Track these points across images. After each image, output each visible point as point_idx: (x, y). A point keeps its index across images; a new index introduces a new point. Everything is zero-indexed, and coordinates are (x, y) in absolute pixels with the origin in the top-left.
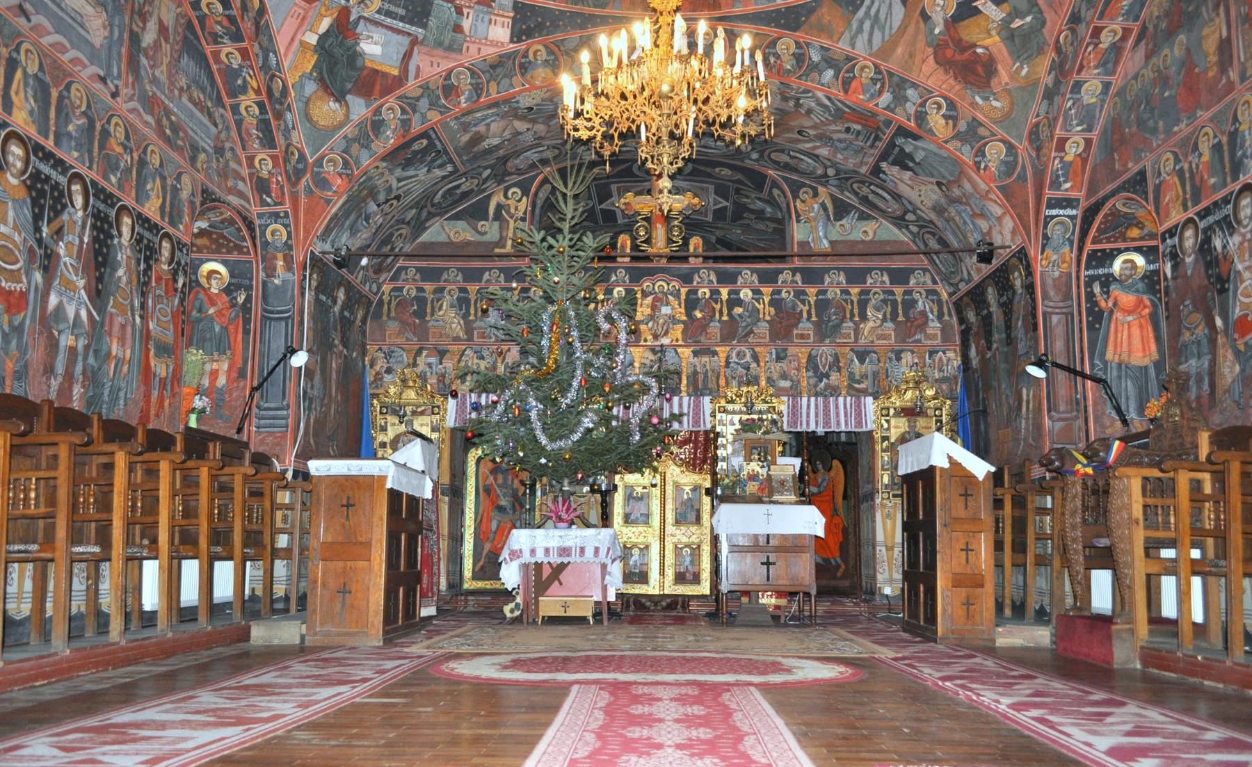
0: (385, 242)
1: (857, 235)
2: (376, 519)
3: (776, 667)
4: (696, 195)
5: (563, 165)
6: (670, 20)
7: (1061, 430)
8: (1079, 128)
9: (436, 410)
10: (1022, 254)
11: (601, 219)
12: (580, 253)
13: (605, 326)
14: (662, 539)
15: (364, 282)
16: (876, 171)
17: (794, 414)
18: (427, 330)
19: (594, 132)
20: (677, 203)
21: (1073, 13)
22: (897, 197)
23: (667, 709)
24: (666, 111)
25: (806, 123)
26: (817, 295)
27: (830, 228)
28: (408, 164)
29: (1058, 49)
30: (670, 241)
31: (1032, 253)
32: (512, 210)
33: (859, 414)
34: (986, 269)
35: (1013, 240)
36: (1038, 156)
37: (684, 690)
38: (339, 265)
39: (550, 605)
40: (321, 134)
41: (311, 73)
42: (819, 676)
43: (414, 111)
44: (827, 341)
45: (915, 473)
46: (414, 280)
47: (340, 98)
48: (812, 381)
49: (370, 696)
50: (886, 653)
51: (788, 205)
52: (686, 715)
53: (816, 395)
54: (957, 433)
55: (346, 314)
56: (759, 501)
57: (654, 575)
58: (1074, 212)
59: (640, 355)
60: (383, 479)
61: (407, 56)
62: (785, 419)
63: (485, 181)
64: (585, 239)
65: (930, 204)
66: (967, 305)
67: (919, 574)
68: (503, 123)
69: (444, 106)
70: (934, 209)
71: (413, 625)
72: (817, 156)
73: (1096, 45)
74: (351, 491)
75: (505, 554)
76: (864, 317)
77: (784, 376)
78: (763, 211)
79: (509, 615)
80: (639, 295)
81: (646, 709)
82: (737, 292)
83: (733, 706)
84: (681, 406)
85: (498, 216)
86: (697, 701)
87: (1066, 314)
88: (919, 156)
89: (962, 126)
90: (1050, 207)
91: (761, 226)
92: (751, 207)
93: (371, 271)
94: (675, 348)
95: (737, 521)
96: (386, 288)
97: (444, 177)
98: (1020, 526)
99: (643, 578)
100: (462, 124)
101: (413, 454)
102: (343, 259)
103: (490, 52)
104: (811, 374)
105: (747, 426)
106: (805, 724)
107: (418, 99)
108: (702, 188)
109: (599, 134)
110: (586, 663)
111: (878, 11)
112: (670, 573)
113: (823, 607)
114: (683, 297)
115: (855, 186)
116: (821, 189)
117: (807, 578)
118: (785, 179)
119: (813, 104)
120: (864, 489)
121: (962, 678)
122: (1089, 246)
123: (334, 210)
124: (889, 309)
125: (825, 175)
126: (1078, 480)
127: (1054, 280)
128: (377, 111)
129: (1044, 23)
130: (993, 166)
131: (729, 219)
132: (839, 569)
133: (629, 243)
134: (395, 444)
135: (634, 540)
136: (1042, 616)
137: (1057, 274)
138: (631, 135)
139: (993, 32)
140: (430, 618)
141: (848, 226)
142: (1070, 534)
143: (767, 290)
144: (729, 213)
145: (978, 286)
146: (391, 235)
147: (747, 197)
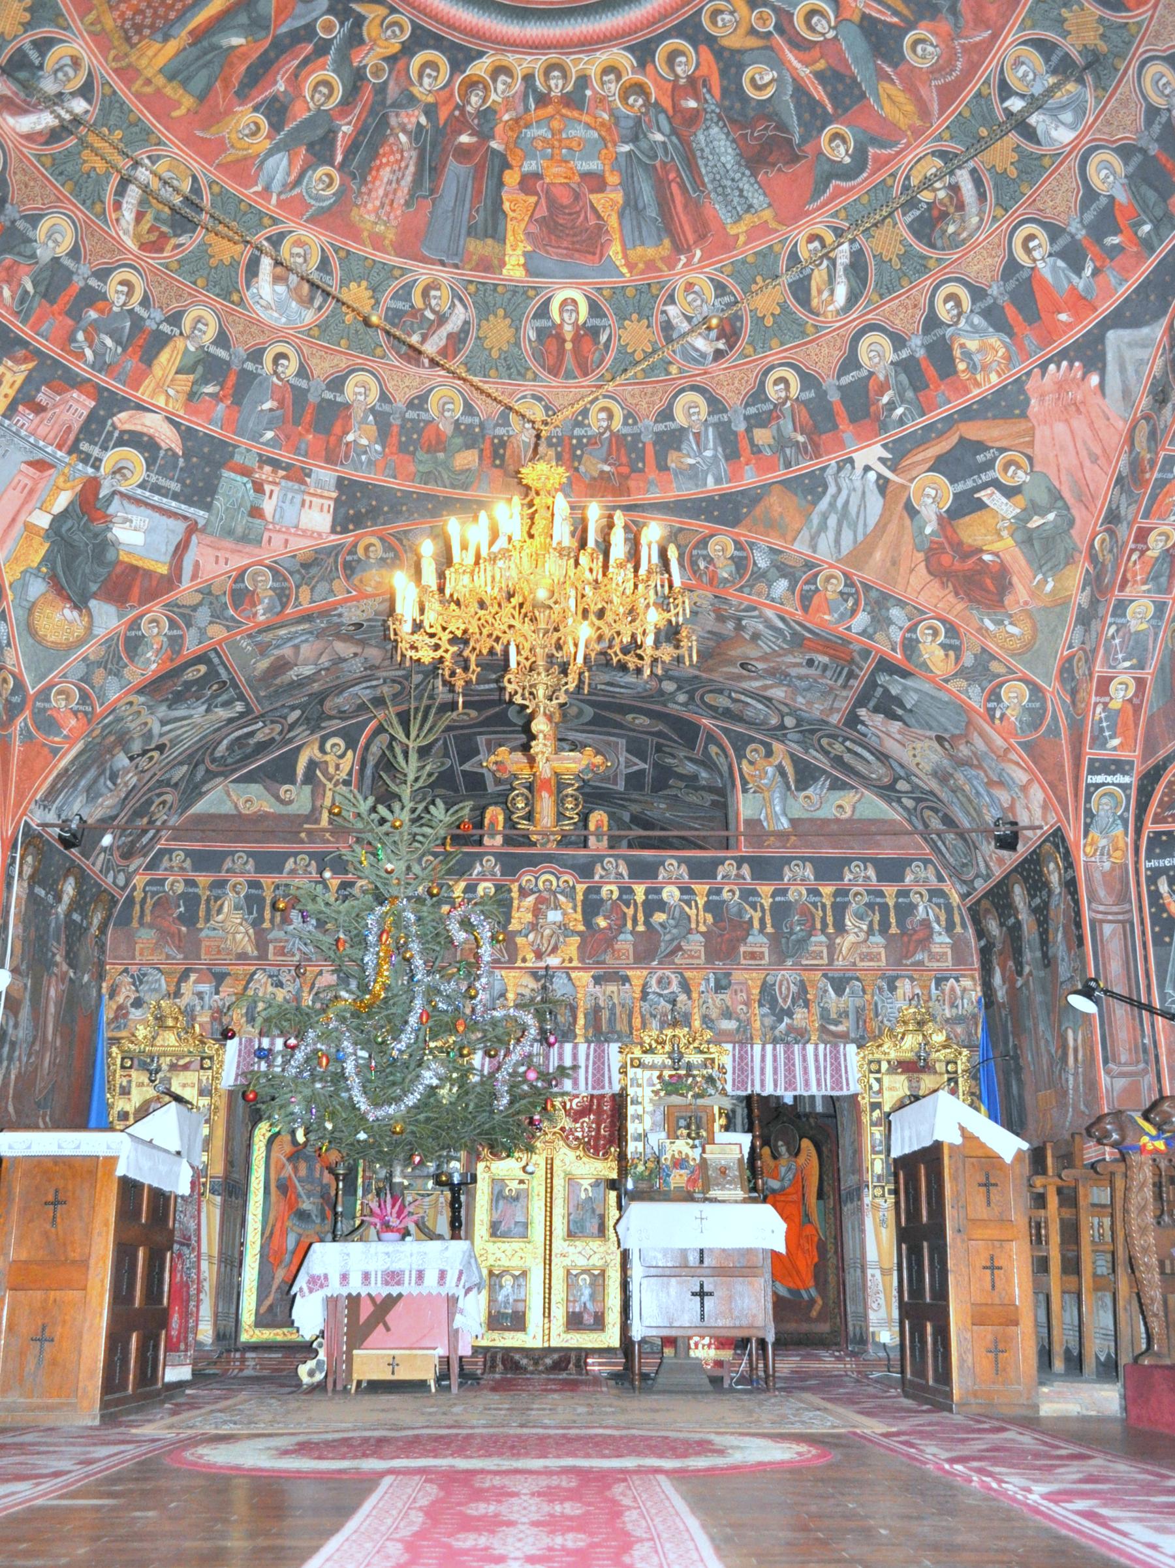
0: (138, 813)
1: (828, 811)
2: (98, 1224)
3: (703, 1447)
4: (598, 752)
5: (404, 707)
6: (549, 501)
7: (1125, 1090)
8: (1127, 664)
9: (207, 1063)
10: (1057, 838)
11: (461, 784)
12: (427, 830)
13: (460, 936)
14: (548, 1261)
15: (106, 869)
16: (853, 720)
17: (742, 1070)
18: (197, 943)
19: (440, 653)
20: (573, 763)
21: (1110, 510)
22: (883, 757)
23: (525, 1507)
24: (542, 625)
25: (753, 652)
26: (773, 896)
27: (791, 801)
28: (177, 699)
29: (1093, 557)
30: (560, 816)
31: (1071, 835)
32: (331, 770)
33: (837, 1069)
34: (1011, 859)
35: (1044, 817)
36: (1073, 703)
37: (555, 1481)
38: (67, 843)
39: (370, 1363)
40: (49, 655)
41: (38, 569)
42: (766, 1458)
43: (189, 625)
44: (789, 963)
45: (914, 1154)
46: (182, 869)
47: (80, 604)
48: (769, 1021)
49: (61, 1497)
50: (873, 1427)
51: (730, 767)
52: (552, 1516)
53: (775, 1041)
54: (980, 1098)
55: (76, 917)
56: (689, 1198)
57: (534, 1317)
58: (1126, 780)
59: (517, 983)
60: (112, 1161)
61: (181, 548)
62: (729, 1077)
63: (292, 727)
64: (432, 808)
65: (928, 768)
66: (987, 911)
67: (924, 1310)
68: (319, 645)
69: (233, 619)
70: (935, 774)
71: (147, 1396)
72: (770, 699)
73: (1143, 553)
74: (61, 1181)
75: (301, 1282)
76: (841, 929)
77: (727, 1014)
78: (695, 777)
79: (306, 1379)
80: (515, 895)
81: (492, 1508)
82: (658, 891)
83: (627, 1501)
84: (575, 1056)
85: (309, 778)
86: (573, 1495)
87: (1122, 922)
88: (910, 700)
89: (968, 660)
90: (1093, 771)
91: (693, 798)
92: (680, 770)
93: (116, 854)
94: (567, 971)
95: (657, 1229)
96: (139, 880)
97: (231, 721)
98: (1071, 1232)
99: (518, 1322)
100: (258, 644)
101: (165, 1127)
102: (74, 835)
103: (301, 544)
104: (766, 1010)
105: (672, 1086)
106: (730, 1525)
107: (194, 608)
108: (609, 744)
109: (448, 656)
110: (412, 1446)
111: (847, 502)
112: (559, 1314)
113: (786, 1365)
114: (580, 897)
115: (824, 741)
116: (777, 746)
117: (761, 1316)
118: (726, 731)
119: (761, 627)
120: (848, 1181)
121: (980, 1459)
122: (1150, 827)
123: (63, 763)
124: (877, 917)
125: (782, 727)
126: (1146, 1159)
127: (1104, 874)
128: (135, 624)
129: (1072, 523)
130: (1012, 715)
131: (647, 789)
132: (811, 1308)
133: (501, 818)
134: (143, 1112)
135: (505, 1262)
136: (1109, 1370)
137: (1107, 866)
138: (497, 664)
139: (1005, 533)
140: (180, 1385)
141: (815, 798)
142: (1138, 1242)
143: (701, 889)
144: (648, 779)
145: (999, 885)
146: (149, 802)
147: (673, 756)
